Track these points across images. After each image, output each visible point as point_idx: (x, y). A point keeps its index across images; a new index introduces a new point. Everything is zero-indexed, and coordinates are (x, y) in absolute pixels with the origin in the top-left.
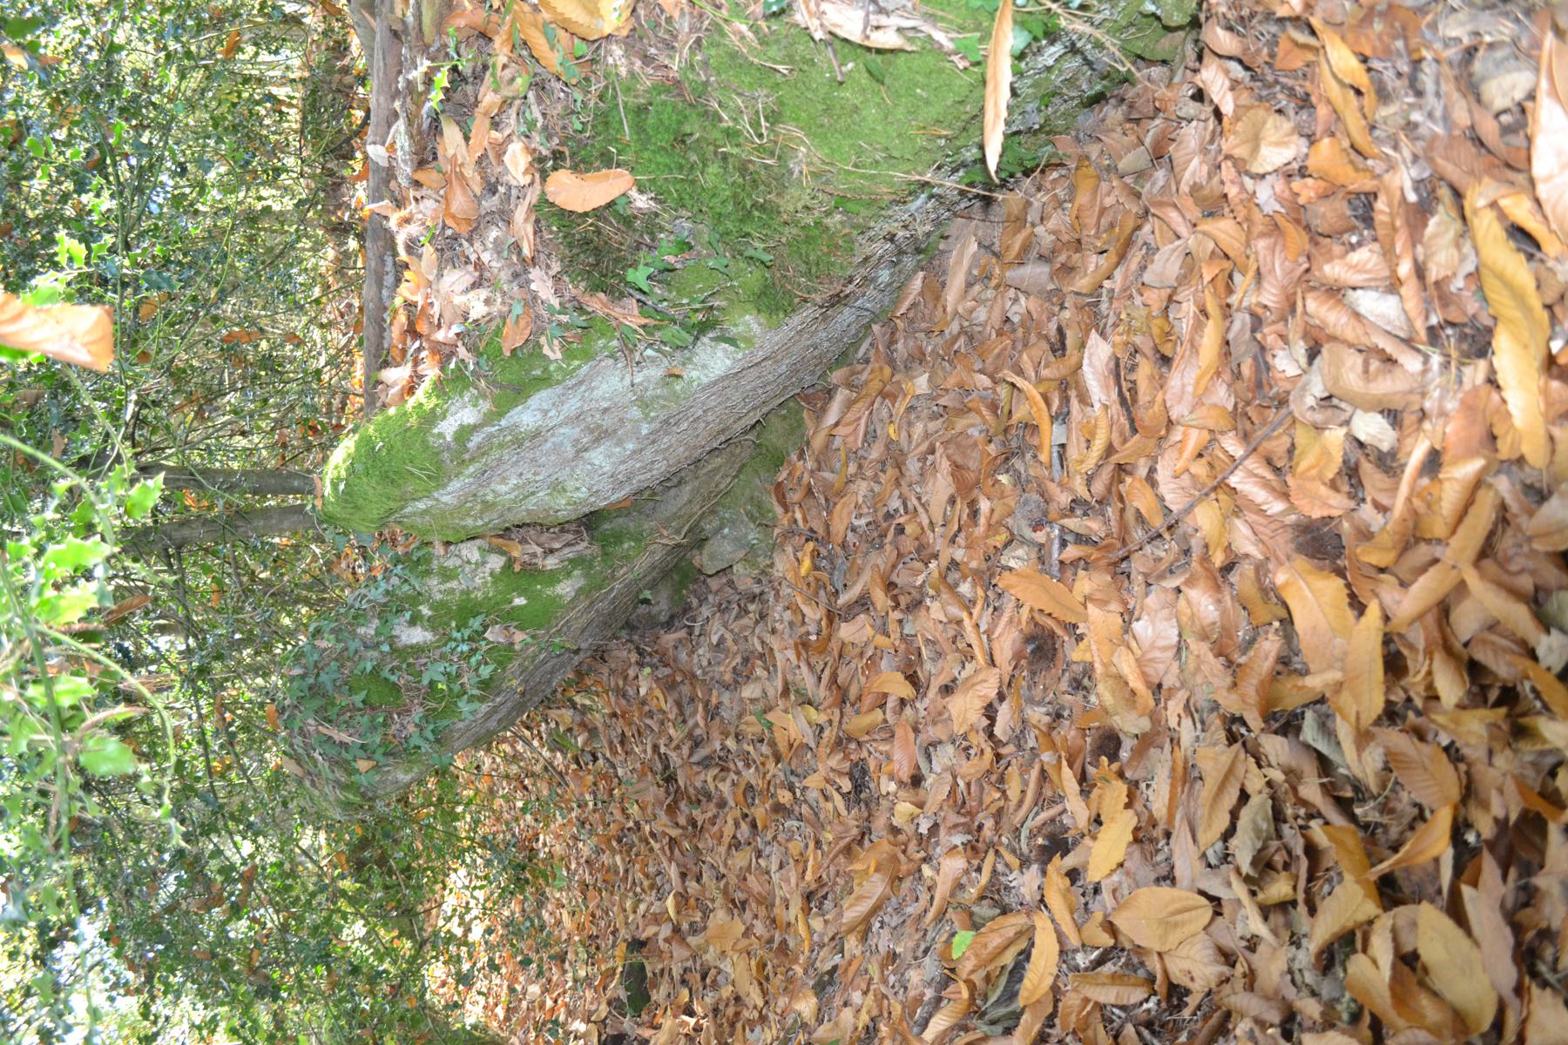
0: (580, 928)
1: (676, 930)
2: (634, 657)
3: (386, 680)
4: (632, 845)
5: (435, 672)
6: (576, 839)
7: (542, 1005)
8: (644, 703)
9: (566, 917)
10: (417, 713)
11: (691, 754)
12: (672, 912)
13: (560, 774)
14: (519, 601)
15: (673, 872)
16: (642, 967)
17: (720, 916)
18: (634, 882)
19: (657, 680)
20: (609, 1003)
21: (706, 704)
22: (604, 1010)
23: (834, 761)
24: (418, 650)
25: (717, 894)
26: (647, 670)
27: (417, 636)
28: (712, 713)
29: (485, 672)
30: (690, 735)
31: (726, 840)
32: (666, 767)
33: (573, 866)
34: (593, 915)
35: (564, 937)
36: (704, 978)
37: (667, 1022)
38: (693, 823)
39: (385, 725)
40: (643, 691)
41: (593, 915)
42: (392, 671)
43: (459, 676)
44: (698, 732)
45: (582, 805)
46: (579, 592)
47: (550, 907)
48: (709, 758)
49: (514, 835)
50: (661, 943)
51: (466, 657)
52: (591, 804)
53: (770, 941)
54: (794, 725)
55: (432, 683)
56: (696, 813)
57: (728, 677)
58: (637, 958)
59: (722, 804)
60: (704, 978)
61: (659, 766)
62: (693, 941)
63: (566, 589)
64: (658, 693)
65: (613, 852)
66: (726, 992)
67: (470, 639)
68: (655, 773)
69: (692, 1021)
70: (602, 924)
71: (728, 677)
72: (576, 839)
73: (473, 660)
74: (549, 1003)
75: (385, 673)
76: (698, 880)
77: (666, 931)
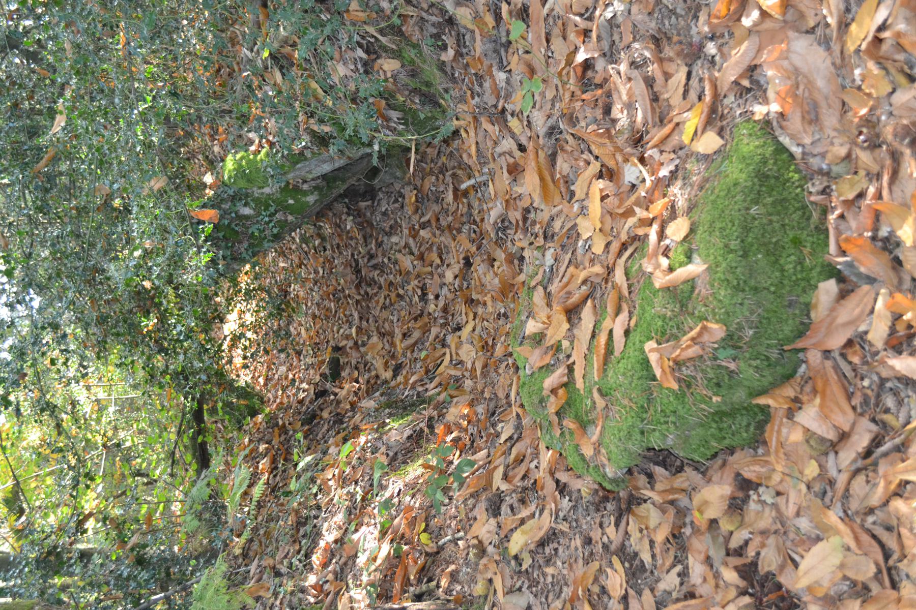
0: (311, 338)
1: (356, 343)
2: (345, 210)
3: (233, 229)
4: (340, 299)
5: (254, 229)
6: (312, 290)
7: (286, 378)
8: (348, 232)
9: (303, 332)
10: (246, 244)
11: (369, 261)
12: (354, 335)
13: (306, 253)
14: (291, 202)
15: (356, 315)
16: (338, 360)
17: (375, 339)
18: (339, 318)
19: (355, 223)
20: (321, 375)
21: (377, 240)
22: (318, 378)
23: (416, 282)
24: (247, 217)
25: (373, 329)
26: (351, 218)
27: (247, 211)
28: (379, 245)
29: (275, 231)
30: (369, 253)
31: (380, 304)
32: (357, 265)
33: (309, 304)
34: (318, 332)
35: (302, 342)
36: (365, 367)
37: (347, 386)
38: (367, 293)
39: (232, 247)
40: (348, 227)
41: (318, 332)
42: (236, 225)
43: (264, 231)
44: (372, 252)
45: (316, 272)
46: (316, 201)
47: (295, 325)
48: (377, 264)
49: (276, 281)
50: (348, 349)
51: (268, 223)
52: (321, 272)
53: (390, 352)
54: (407, 262)
55: (253, 233)
56: (369, 290)
57: (387, 229)
58: (337, 355)
59: (380, 288)
60: (365, 367)
61: (354, 265)
62: (362, 349)
63: (311, 199)
64: (355, 230)
65: (330, 300)
66: (373, 373)
67: (270, 216)
68: (351, 266)
69: (357, 385)
70: (322, 337)
71: (387, 229)
72: (312, 290)
73: (271, 225)
74: (291, 376)
75: (233, 226)
76: (368, 322)
77: (350, 343)
